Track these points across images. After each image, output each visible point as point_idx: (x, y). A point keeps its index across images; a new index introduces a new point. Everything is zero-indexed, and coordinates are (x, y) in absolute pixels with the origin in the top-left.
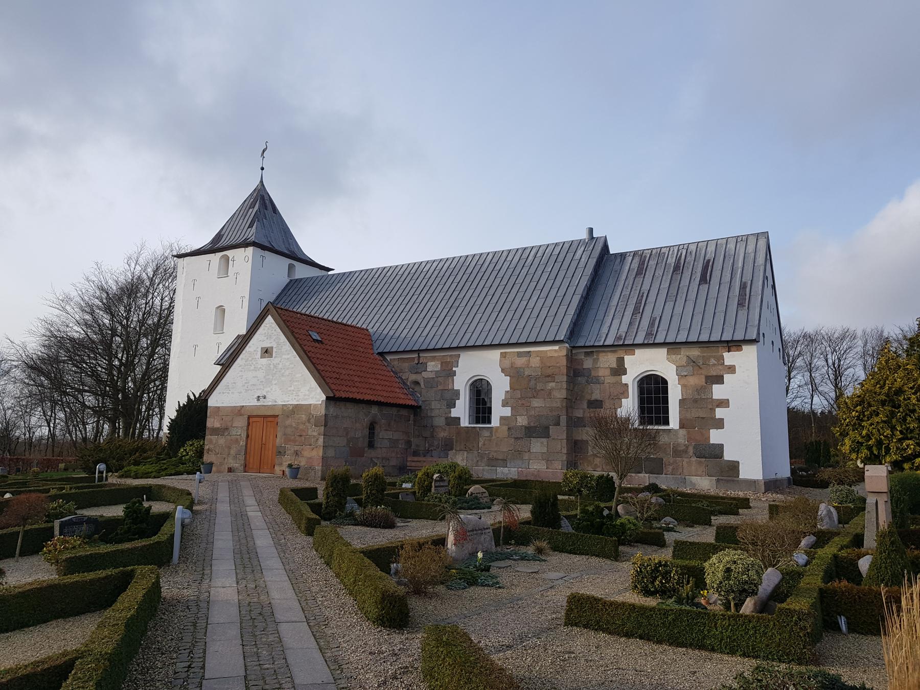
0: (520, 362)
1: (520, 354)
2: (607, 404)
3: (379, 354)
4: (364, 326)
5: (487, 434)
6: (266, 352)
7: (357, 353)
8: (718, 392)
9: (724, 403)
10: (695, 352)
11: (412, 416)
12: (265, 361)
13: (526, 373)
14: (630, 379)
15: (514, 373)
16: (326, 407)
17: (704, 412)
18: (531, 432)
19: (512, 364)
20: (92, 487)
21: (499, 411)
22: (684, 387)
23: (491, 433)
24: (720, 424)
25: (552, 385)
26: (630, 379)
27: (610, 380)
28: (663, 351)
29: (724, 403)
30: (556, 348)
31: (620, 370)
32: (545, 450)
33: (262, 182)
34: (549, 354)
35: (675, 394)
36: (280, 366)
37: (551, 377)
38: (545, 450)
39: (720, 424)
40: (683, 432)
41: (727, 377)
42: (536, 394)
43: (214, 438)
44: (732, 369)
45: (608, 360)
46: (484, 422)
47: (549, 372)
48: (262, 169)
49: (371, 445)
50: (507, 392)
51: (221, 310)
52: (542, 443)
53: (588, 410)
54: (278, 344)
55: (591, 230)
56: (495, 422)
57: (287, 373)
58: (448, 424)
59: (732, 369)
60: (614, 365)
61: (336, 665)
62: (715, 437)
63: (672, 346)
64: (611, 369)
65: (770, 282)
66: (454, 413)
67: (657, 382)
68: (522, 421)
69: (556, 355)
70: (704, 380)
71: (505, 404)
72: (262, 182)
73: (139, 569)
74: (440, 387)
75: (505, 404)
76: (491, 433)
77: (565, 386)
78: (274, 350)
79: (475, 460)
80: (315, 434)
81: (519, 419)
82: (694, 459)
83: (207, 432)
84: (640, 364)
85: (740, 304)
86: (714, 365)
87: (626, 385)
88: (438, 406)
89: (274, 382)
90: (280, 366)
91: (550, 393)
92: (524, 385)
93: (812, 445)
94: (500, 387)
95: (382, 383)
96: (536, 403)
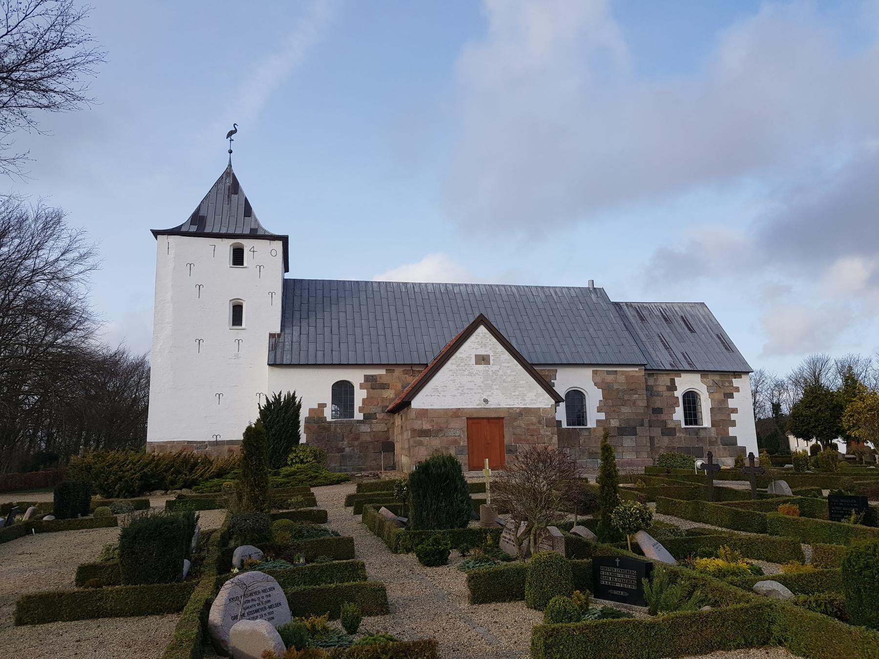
0: (610, 378)
1: (608, 372)
2: (666, 411)
5: (586, 433)
8: (731, 403)
9: (735, 411)
10: (717, 378)
12: (481, 367)
13: (615, 387)
14: (679, 393)
15: (606, 388)
17: (723, 416)
19: (603, 380)
21: (593, 416)
24: (733, 423)
25: (636, 396)
26: (679, 393)
27: (667, 394)
28: (698, 377)
29: (735, 411)
30: (637, 369)
31: (673, 387)
32: (634, 444)
33: (230, 165)
34: (631, 374)
36: (501, 373)
37: (634, 391)
38: (634, 444)
39: (733, 423)
40: (714, 429)
41: (735, 394)
45: (664, 380)
47: (633, 387)
48: (231, 152)
50: (600, 401)
54: (495, 353)
55: (238, 257)
57: (509, 379)
60: (669, 384)
62: (732, 431)
63: (704, 373)
64: (667, 386)
68: (614, 423)
69: (637, 374)
71: (599, 410)
72: (230, 165)
75: (599, 410)
78: (491, 358)
80: (548, 433)
81: (612, 422)
82: (721, 446)
84: (685, 383)
85: (667, 349)
89: (495, 387)
90: (501, 373)
92: (613, 398)
93: (771, 432)
94: (594, 397)
96: (625, 410)
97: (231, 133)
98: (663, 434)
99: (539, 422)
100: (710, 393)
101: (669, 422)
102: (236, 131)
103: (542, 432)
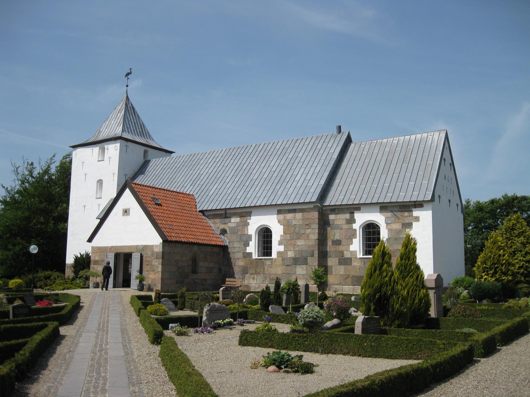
2: (343, 242)
3: (200, 211)
4: (191, 193)
6: (126, 212)
7: (185, 211)
11: (221, 253)
13: (294, 223)
14: (357, 226)
15: (287, 226)
16: (163, 247)
18: (296, 261)
20: (7, 323)
21: (276, 248)
22: (390, 230)
23: (272, 262)
26: (357, 226)
27: (345, 227)
31: (352, 221)
32: (305, 272)
35: (276, 238)
38: (305, 272)
41: (415, 224)
42: (299, 236)
43: (95, 266)
44: (417, 219)
46: (267, 255)
48: (127, 86)
49: (194, 272)
50: (281, 236)
51: (100, 182)
52: (303, 268)
53: (332, 246)
56: (274, 255)
58: (244, 257)
59: (417, 219)
61: (128, 353)
65: (448, 161)
66: (249, 250)
67: (374, 228)
68: (291, 254)
70: (401, 226)
71: (280, 243)
73: (49, 323)
74: (239, 233)
75: (280, 243)
76: (272, 262)
77: (317, 231)
79: (262, 280)
83: (92, 263)
86: (407, 216)
87: (355, 230)
88: (238, 246)
91: (308, 236)
94: (277, 232)
95: (201, 231)
96: (300, 242)
97: (128, 74)
98: (340, 263)
99: (152, 256)
100: (387, 224)
101: (345, 253)
102: (131, 73)
103: (153, 263)
